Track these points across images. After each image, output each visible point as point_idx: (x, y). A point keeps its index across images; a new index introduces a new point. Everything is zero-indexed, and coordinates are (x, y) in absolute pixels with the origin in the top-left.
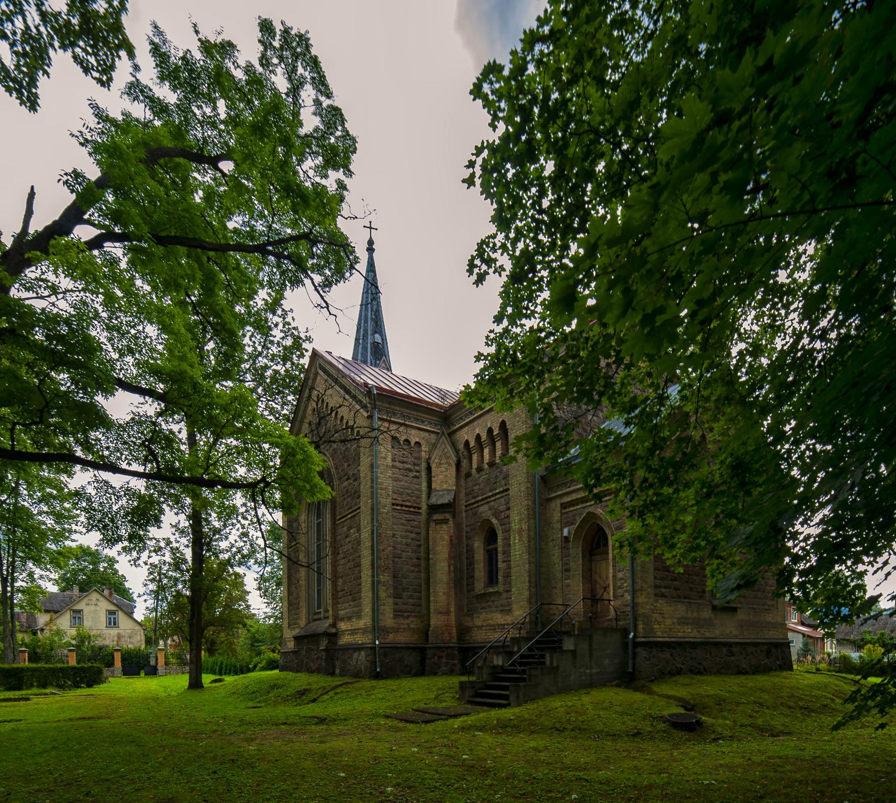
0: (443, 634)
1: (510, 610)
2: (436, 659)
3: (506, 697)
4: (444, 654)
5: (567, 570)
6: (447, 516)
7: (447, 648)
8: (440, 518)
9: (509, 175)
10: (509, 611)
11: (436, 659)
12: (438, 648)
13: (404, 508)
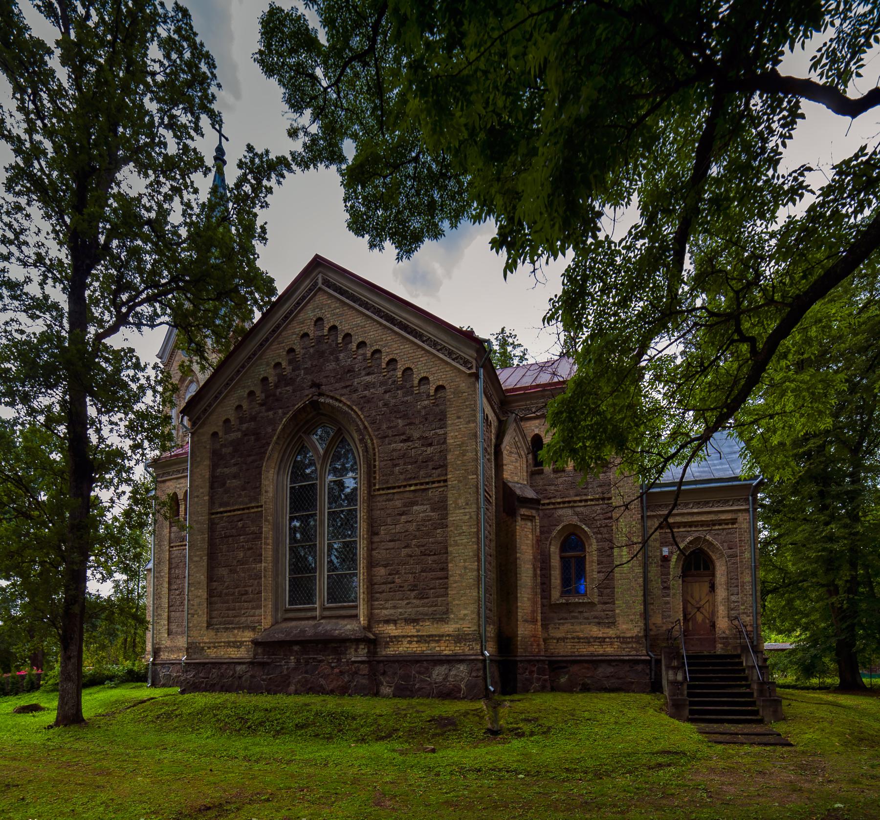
0: (532, 645)
1: (614, 623)
2: (527, 675)
3: (756, 713)
4: (535, 669)
5: (667, 588)
6: (534, 512)
7: (538, 661)
8: (526, 513)
9: (469, 178)
10: (613, 624)
11: (527, 675)
12: (529, 661)
13: (418, 487)
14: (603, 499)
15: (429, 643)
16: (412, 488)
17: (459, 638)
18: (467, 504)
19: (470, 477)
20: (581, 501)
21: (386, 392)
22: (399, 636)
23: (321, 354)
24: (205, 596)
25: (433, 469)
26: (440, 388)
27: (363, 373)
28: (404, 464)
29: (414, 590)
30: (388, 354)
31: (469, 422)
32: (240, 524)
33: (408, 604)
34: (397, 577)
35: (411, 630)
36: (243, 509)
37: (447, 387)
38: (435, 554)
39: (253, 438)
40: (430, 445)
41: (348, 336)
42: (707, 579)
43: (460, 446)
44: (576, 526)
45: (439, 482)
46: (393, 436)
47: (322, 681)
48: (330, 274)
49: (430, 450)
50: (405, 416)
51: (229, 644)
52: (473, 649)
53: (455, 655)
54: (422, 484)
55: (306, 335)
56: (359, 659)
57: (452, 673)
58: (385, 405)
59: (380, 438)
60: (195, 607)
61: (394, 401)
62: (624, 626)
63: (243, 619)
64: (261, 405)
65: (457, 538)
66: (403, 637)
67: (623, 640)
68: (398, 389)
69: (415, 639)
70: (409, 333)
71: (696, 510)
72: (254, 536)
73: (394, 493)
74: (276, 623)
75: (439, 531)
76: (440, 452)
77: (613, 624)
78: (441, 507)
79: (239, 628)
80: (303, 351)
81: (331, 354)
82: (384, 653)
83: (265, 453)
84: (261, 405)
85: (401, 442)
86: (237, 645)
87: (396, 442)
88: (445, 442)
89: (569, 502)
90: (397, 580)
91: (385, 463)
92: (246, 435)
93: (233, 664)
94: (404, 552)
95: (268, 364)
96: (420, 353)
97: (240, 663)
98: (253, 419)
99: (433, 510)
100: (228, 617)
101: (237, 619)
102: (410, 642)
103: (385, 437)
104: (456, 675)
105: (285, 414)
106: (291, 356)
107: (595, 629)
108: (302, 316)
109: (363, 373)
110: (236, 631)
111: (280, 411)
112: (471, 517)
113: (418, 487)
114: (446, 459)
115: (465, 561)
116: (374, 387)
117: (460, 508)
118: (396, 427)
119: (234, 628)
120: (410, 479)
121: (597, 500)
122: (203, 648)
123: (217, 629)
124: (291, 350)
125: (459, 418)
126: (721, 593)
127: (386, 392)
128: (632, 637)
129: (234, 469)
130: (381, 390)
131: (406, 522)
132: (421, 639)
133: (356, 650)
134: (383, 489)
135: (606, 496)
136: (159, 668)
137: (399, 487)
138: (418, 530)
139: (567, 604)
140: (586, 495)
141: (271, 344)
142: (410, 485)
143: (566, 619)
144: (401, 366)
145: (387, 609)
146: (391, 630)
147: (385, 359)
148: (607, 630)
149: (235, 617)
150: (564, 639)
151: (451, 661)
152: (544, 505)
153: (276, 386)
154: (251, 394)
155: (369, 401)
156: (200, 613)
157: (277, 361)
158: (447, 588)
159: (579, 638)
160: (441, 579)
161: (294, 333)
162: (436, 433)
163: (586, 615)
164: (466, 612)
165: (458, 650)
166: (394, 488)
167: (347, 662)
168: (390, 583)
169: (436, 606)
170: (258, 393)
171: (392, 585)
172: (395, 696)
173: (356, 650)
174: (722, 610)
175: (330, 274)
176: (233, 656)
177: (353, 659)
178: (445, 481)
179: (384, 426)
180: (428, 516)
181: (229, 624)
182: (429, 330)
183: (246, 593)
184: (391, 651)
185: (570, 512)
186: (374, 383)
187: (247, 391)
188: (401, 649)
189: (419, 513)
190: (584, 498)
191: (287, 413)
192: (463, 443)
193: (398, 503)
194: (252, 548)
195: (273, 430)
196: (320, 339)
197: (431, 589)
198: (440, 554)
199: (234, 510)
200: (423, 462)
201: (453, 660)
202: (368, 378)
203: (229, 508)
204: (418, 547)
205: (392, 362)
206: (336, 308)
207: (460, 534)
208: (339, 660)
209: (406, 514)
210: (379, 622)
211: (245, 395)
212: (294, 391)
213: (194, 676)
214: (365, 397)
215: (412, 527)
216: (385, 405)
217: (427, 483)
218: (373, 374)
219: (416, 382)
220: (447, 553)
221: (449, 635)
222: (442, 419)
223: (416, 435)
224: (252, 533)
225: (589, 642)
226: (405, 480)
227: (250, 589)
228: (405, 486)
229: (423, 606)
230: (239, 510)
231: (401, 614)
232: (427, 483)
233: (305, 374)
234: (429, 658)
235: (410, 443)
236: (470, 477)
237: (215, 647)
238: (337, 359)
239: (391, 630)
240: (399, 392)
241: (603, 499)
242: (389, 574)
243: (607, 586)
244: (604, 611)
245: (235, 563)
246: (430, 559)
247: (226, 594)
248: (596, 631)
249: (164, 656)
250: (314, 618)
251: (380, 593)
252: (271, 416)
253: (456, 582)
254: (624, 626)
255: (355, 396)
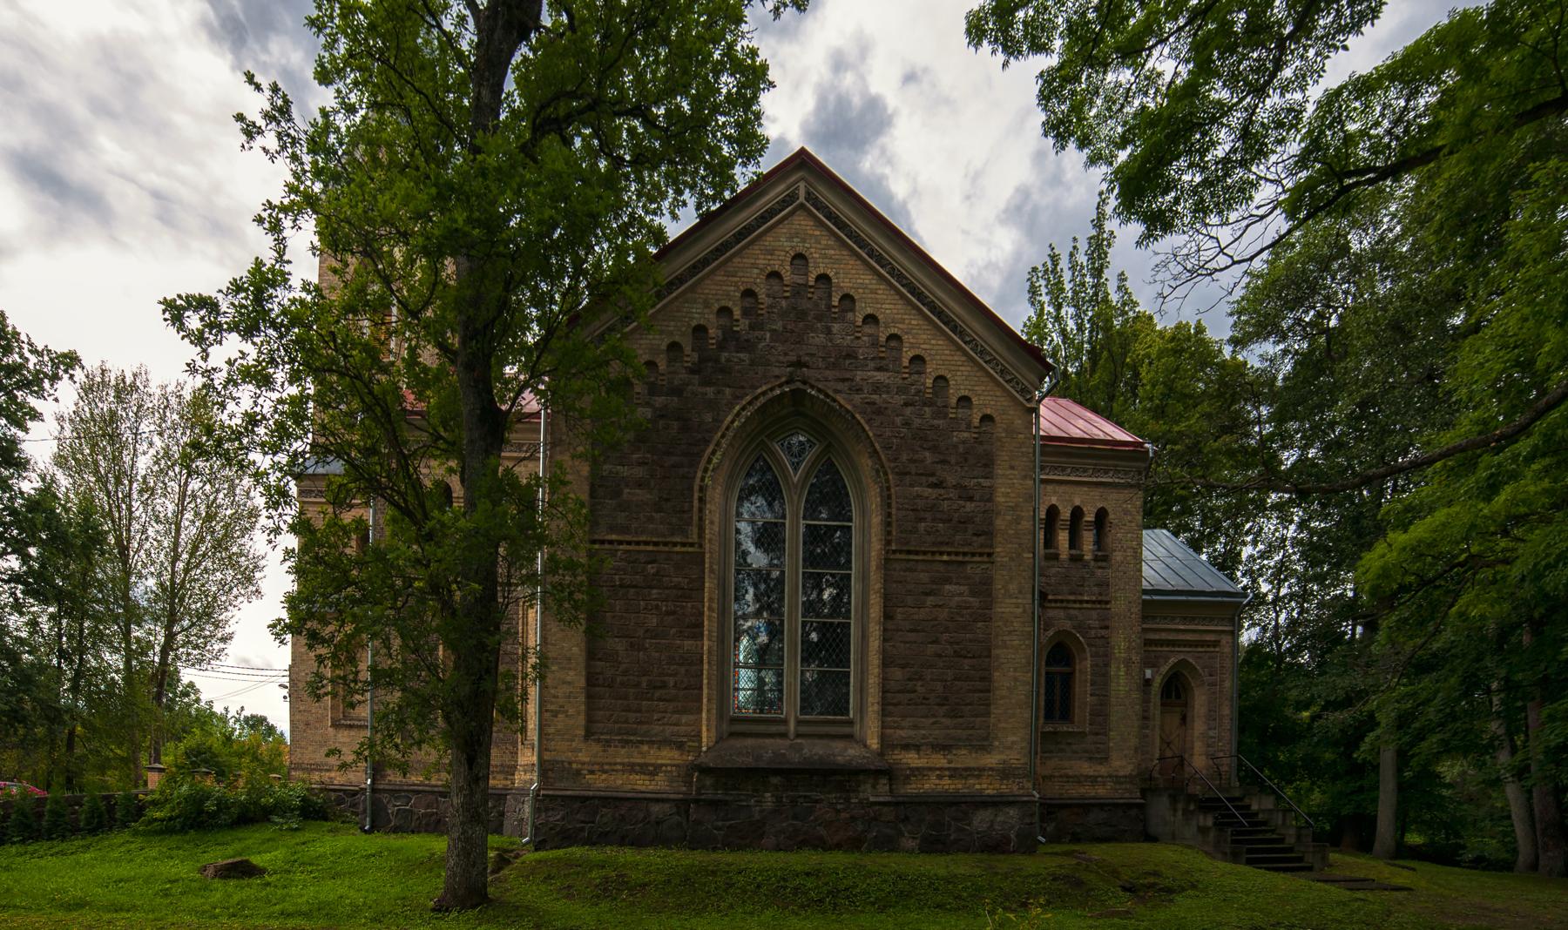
1: (1106, 759)
10: (1105, 760)
14: (1100, 602)
15: (966, 778)
16: (945, 558)
17: (1005, 773)
18: (1020, 592)
19: (1025, 555)
20: (1075, 602)
21: (906, 404)
22: (924, 768)
23: (802, 315)
24: (582, 682)
25: (975, 534)
26: (987, 418)
27: (872, 365)
28: (934, 520)
29: (943, 705)
30: (912, 346)
31: (1025, 477)
32: (651, 569)
33: (934, 723)
34: (920, 683)
35: (940, 760)
36: (656, 544)
37: (997, 419)
38: (974, 657)
39: (675, 425)
40: (971, 499)
41: (847, 298)
42: (1178, 709)
43: (1013, 509)
44: (1070, 633)
45: (981, 555)
46: (917, 474)
47: (822, 831)
48: (820, 188)
49: (970, 506)
50: (934, 449)
51: (632, 768)
52: (1023, 788)
53: (1001, 796)
54: (957, 554)
55: (775, 275)
56: (881, 799)
57: (999, 819)
58: (907, 424)
59: (897, 474)
60: (561, 701)
61: (919, 421)
62: (1118, 763)
63: (657, 728)
64: (692, 371)
65: (1005, 638)
66: (930, 769)
67: (1117, 779)
68: (925, 404)
69: (947, 773)
70: (944, 323)
71: (1182, 627)
72: (680, 593)
73: (917, 561)
74: (719, 739)
75: (980, 624)
76: (984, 512)
77: (1105, 760)
78: (984, 589)
79: (653, 742)
80: (768, 301)
81: (819, 318)
82: (902, 791)
83: (700, 455)
84: (692, 371)
85: (929, 486)
86: (652, 771)
87: (921, 485)
88: (990, 500)
89: (1062, 601)
90: (919, 688)
91: (904, 513)
92: (662, 416)
93: (641, 801)
94: (931, 649)
95: (707, 305)
96: (959, 358)
97: (657, 800)
98: (677, 391)
99: (973, 594)
100: (626, 722)
101: (645, 727)
102: (940, 777)
103: (906, 474)
104: (1005, 822)
105: (738, 398)
106: (749, 301)
107: (1086, 765)
108: (769, 241)
109: (872, 365)
110: (645, 748)
111: (728, 391)
112: (1024, 611)
113: (953, 558)
114: (991, 524)
115: (1015, 670)
116: (888, 393)
117: (1010, 597)
118: (922, 461)
119: (642, 742)
120: (942, 543)
121: (1094, 602)
122: (578, 773)
123: (607, 741)
124: (749, 293)
125: (1012, 468)
126: (1199, 726)
127: (906, 404)
128: (1125, 777)
129: (639, 472)
130: (899, 399)
131: (935, 606)
132: (955, 773)
133: (874, 787)
134: (901, 552)
135: (1104, 598)
136: (385, 798)
137: (925, 553)
138: (952, 620)
139: (1055, 733)
140: (1081, 594)
141: (713, 272)
142: (941, 553)
143: (1051, 752)
144: (931, 370)
145: (903, 728)
146: (912, 759)
147: (907, 354)
148: (1099, 767)
149: (640, 723)
150: (1051, 777)
151: (997, 803)
152: (1050, 601)
153: (722, 346)
154: (674, 347)
155: (879, 411)
156: (571, 711)
157: (723, 303)
158: (989, 705)
159: (1068, 777)
160: (981, 691)
161: (754, 266)
162: (979, 484)
163: (1074, 747)
164: (1015, 739)
165: (1004, 789)
166: (917, 553)
167: (861, 802)
168: (908, 692)
169: (973, 728)
170: (688, 349)
171: (913, 695)
172: (922, 851)
173: (874, 787)
174: (1198, 746)
175: (820, 188)
176: (643, 788)
177: (872, 799)
178: (989, 555)
179: (904, 457)
180: (965, 602)
181: (627, 733)
182: (976, 326)
183: (664, 686)
184: (912, 788)
185: (1062, 614)
186: (888, 386)
187: (667, 341)
188: (927, 786)
189: (953, 596)
190: (1080, 598)
191: (742, 398)
192: (1017, 506)
193: (924, 577)
194: (674, 613)
195: (715, 420)
196: (799, 290)
197: (967, 705)
198: (980, 657)
199: (638, 543)
200: (960, 522)
201: (1001, 803)
202: (880, 376)
203: (628, 538)
204: (951, 643)
205: (918, 359)
206: (828, 247)
207: (1010, 632)
208: (847, 800)
209: (935, 594)
210: (893, 747)
211: (664, 347)
212: (753, 363)
213: (563, 819)
214: (874, 403)
215: (943, 614)
216: (907, 424)
217: (965, 554)
218: (887, 370)
219: (953, 401)
220: (989, 656)
221: (991, 769)
222: (987, 464)
223: (951, 480)
224: (675, 587)
225: (1079, 782)
226: (934, 544)
227: (671, 680)
228: (933, 553)
229: (955, 728)
230: (646, 543)
231: (924, 737)
232: (965, 554)
233: (772, 340)
234: (969, 799)
235: (942, 491)
236: (1025, 555)
237: (605, 772)
238: (829, 331)
239: (912, 759)
240: (926, 409)
241: (1100, 602)
242: (909, 680)
243: (1100, 713)
244: (1096, 743)
245: (641, 632)
246: (966, 664)
247: (622, 684)
248: (1086, 768)
249: (394, 777)
250: (784, 735)
251: (895, 705)
252: (711, 396)
253: (1003, 698)
254: (1118, 763)
255: (857, 398)
